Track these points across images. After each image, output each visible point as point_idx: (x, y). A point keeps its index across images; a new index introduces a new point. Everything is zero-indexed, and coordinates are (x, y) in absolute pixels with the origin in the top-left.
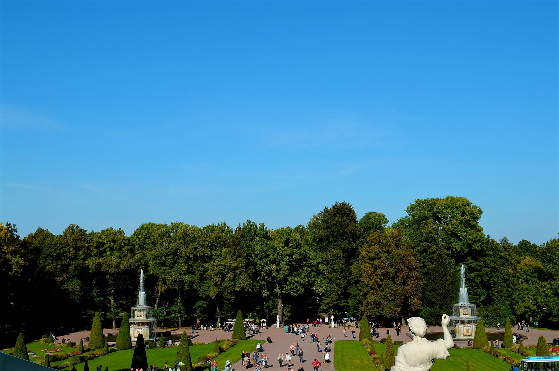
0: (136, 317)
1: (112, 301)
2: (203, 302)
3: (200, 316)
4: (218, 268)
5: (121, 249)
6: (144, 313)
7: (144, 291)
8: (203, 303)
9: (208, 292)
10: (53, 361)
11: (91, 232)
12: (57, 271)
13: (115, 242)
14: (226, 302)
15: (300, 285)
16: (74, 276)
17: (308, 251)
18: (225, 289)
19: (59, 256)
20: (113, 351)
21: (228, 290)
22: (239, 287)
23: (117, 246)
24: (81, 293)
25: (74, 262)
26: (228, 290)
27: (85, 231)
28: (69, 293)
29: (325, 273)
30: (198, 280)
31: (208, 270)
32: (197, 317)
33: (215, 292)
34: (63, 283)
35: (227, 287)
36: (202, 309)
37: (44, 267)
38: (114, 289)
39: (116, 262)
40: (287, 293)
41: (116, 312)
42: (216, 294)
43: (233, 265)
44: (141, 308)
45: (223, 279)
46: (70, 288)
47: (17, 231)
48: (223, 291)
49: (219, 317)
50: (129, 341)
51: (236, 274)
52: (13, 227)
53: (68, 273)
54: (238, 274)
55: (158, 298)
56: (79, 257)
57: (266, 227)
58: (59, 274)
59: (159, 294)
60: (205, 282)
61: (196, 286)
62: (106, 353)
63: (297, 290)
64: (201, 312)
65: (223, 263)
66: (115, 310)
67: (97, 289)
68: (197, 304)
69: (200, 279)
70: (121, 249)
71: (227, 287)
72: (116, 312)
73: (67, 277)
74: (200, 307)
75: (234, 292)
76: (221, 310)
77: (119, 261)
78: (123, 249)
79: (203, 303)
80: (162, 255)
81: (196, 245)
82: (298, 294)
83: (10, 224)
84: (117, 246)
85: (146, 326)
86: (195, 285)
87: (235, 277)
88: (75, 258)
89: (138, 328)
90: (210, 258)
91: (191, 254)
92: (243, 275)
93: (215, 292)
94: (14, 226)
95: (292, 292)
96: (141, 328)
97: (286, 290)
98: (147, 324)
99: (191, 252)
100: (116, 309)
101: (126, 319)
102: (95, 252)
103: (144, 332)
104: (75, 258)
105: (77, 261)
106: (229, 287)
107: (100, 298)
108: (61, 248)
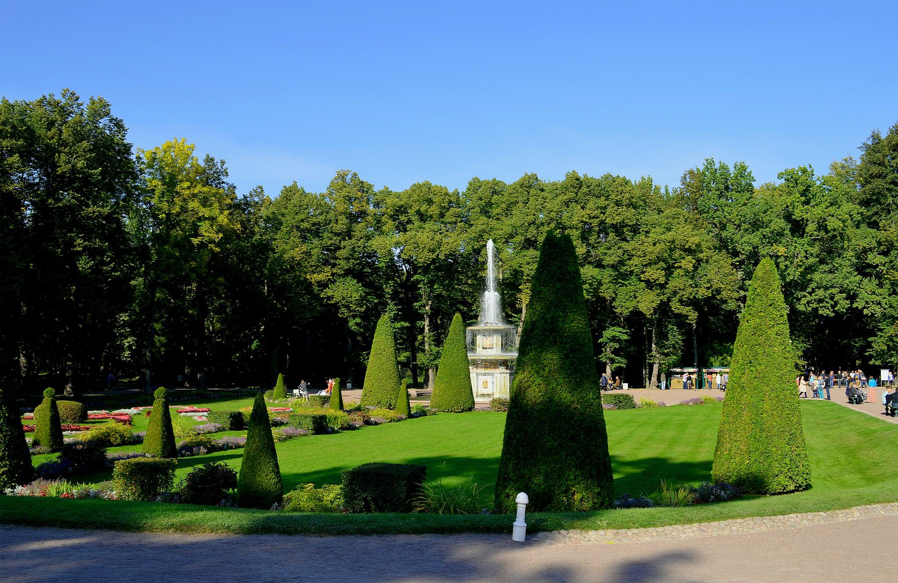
0: (479, 350)
1: (427, 329)
2: (620, 329)
3: (613, 361)
4: (659, 247)
5: (442, 215)
6: (497, 340)
7: (496, 290)
8: (619, 332)
9: (634, 303)
10: (231, 429)
11: (382, 188)
12: (312, 261)
13: (430, 202)
14: (673, 328)
15: (841, 292)
16: (348, 272)
17: (858, 213)
18: (675, 293)
19: (316, 231)
20: (422, 413)
21: (683, 295)
22: (708, 288)
23: (434, 210)
24: (361, 307)
25: (346, 243)
26: (683, 295)
27: (370, 187)
28: (336, 307)
29: (882, 271)
30: (610, 276)
31: (631, 257)
32: (605, 364)
33: (653, 302)
34: (323, 285)
35: (680, 290)
36: (617, 346)
37: (284, 251)
38: (430, 303)
39: (433, 239)
40: (810, 309)
41: (434, 351)
42: (654, 305)
43: (692, 240)
44: (489, 327)
45: (669, 270)
46: (337, 297)
47: (227, 173)
48: (669, 300)
49: (657, 362)
50: (468, 391)
51: (699, 261)
52: (219, 165)
53: (334, 265)
54: (703, 262)
55: (521, 324)
56: (357, 234)
57: (748, 170)
58: (317, 266)
59: (523, 315)
60: (626, 283)
61: (606, 293)
62: (404, 417)
63: (832, 302)
64: (616, 352)
65: (669, 236)
66: (433, 347)
67: (396, 305)
68: (608, 333)
69: (616, 276)
70: (442, 215)
71: (680, 290)
72: (434, 351)
73: (333, 274)
74: (614, 339)
75: (694, 303)
76: (660, 345)
77: (438, 237)
78: (448, 214)
79: (619, 332)
80: (530, 224)
81: (602, 202)
82: (834, 311)
83: (212, 160)
84: (434, 210)
85: (502, 369)
86: (604, 287)
87: (696, 268)
88: (348, 234)
89: (485, 375)
90: (635, 230)
91: (593, 218)
92: (715, 262)
93: (653, 302)
94: (223, 163)
95: (822, 307)
96: (493, 374)
97: (808, 303)
98: (505, 363)
99: (592, 215)
100: (435, 346)
101: (457, 331)
102: (389, 225)
103: (498, 383)
104: (348, 234)
105: (353, 241)
106: (683, 290)
107: (403, 323)
108: (321, 214)
